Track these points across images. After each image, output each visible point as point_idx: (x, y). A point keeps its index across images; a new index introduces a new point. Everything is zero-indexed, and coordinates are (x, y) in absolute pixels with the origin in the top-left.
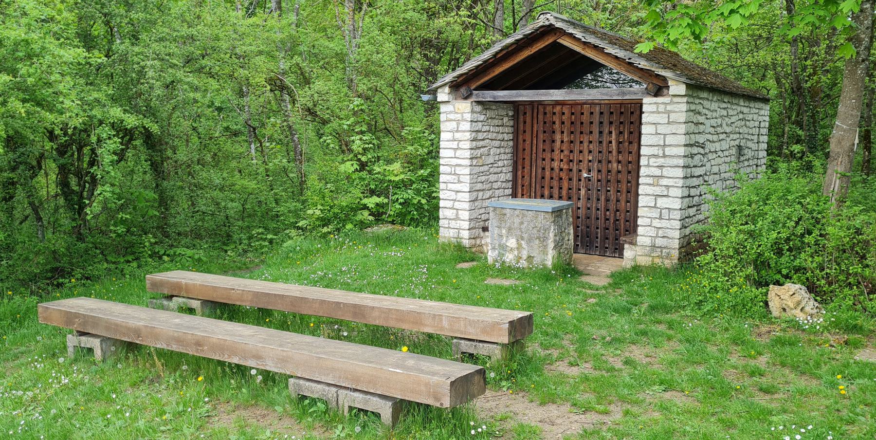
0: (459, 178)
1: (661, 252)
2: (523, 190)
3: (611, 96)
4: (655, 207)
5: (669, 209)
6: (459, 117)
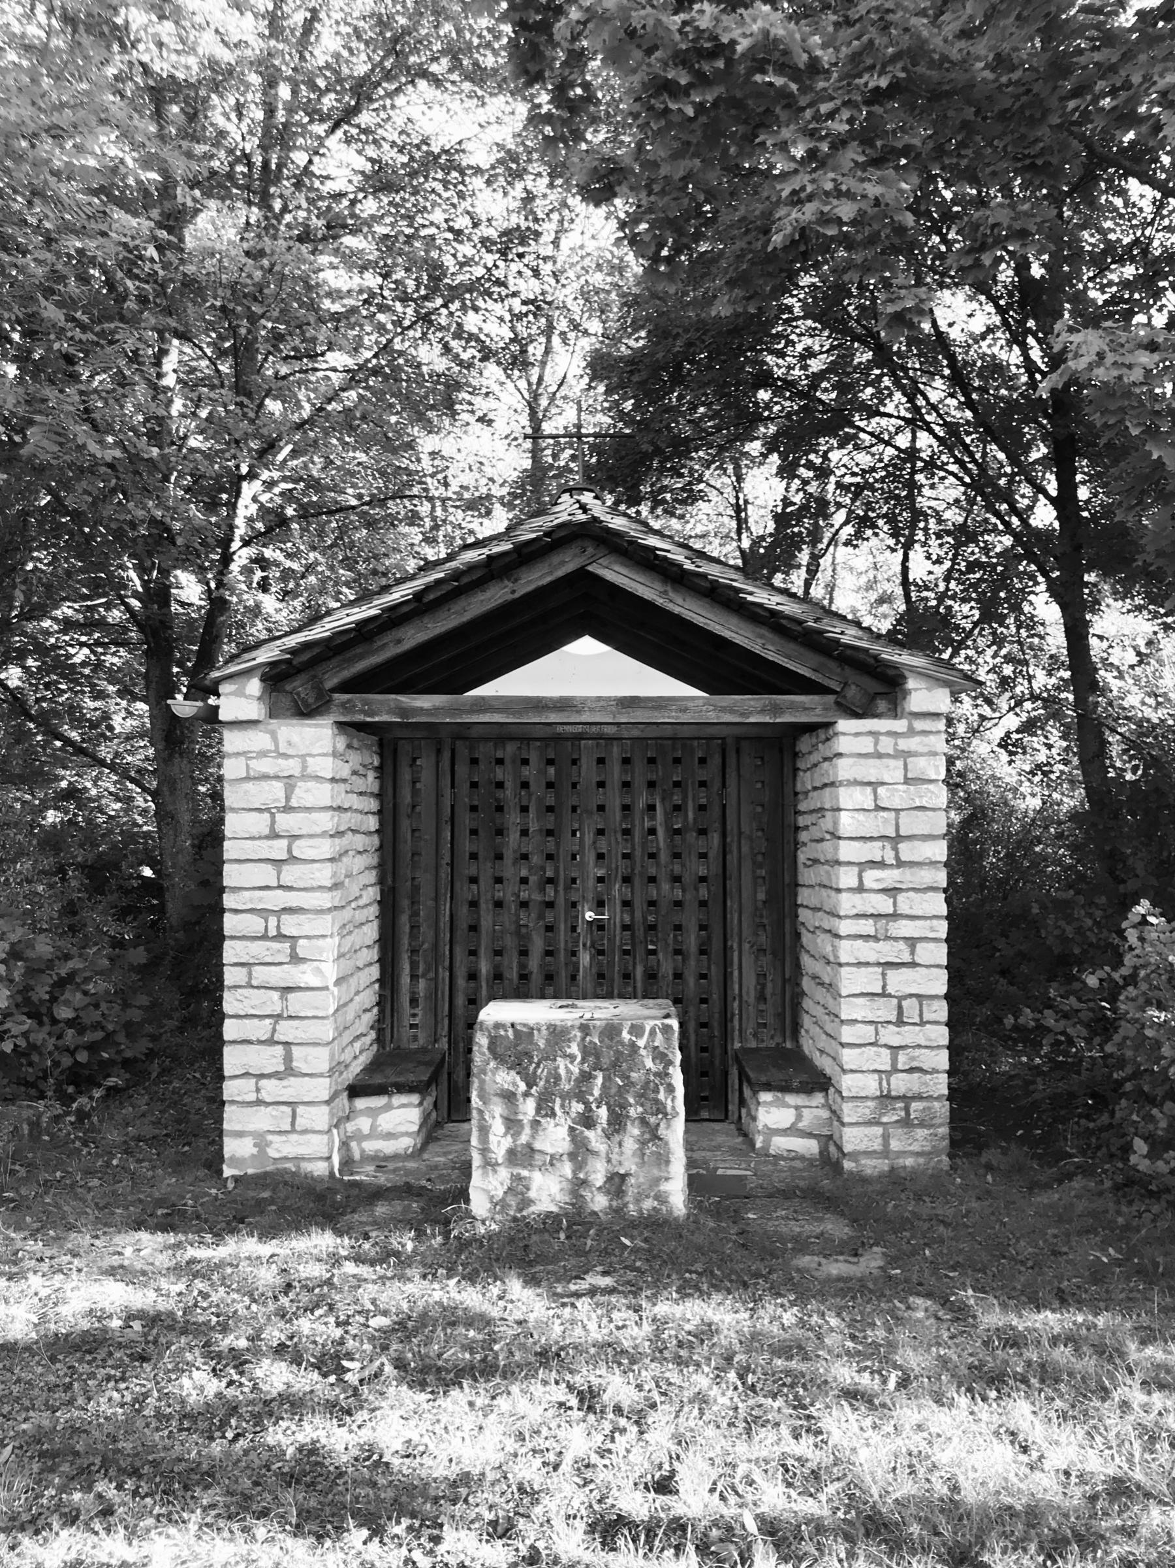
0: (293, 948)
1: (907, 1109)
2: (414, 965)
3: (742, 715)
4: (884, 994)
5: (917, 996)
6: (292, 767)
